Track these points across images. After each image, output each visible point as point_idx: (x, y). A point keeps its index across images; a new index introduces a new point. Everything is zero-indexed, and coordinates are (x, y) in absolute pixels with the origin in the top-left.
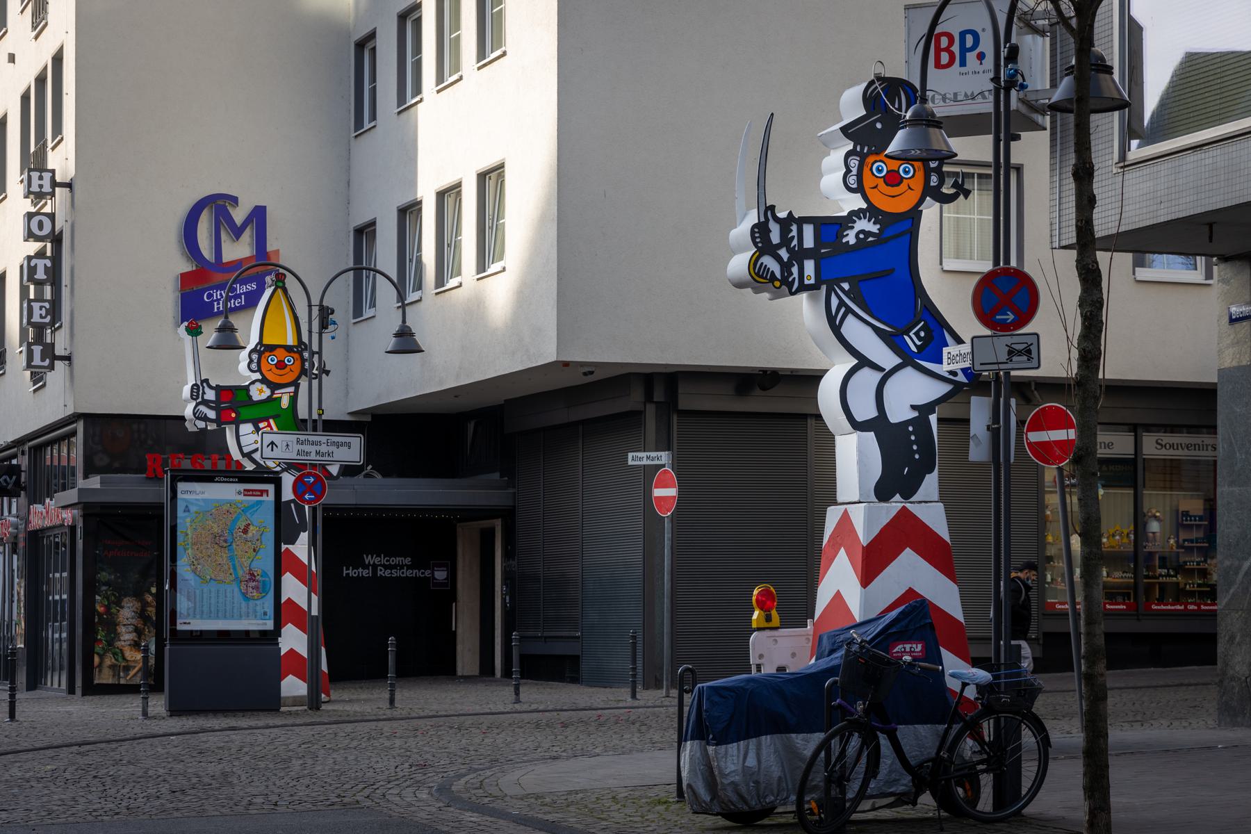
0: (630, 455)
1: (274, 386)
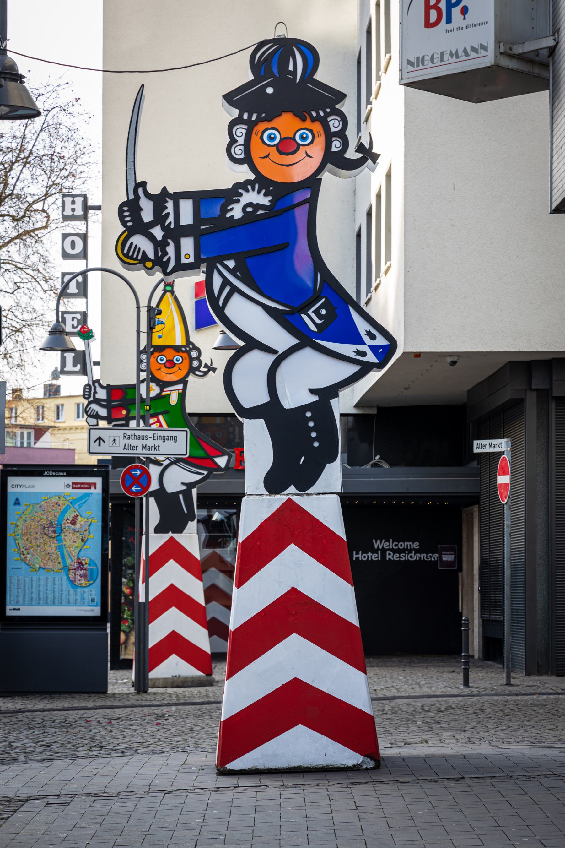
0: (475, 442)
1: (163, 385)
